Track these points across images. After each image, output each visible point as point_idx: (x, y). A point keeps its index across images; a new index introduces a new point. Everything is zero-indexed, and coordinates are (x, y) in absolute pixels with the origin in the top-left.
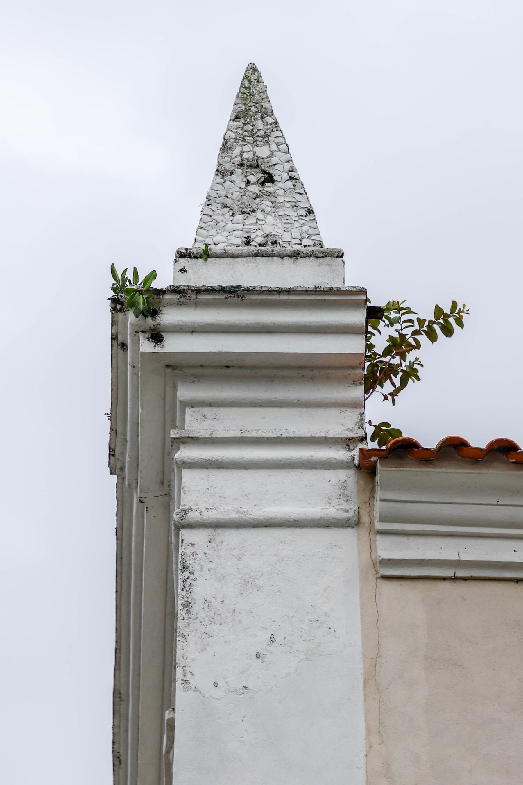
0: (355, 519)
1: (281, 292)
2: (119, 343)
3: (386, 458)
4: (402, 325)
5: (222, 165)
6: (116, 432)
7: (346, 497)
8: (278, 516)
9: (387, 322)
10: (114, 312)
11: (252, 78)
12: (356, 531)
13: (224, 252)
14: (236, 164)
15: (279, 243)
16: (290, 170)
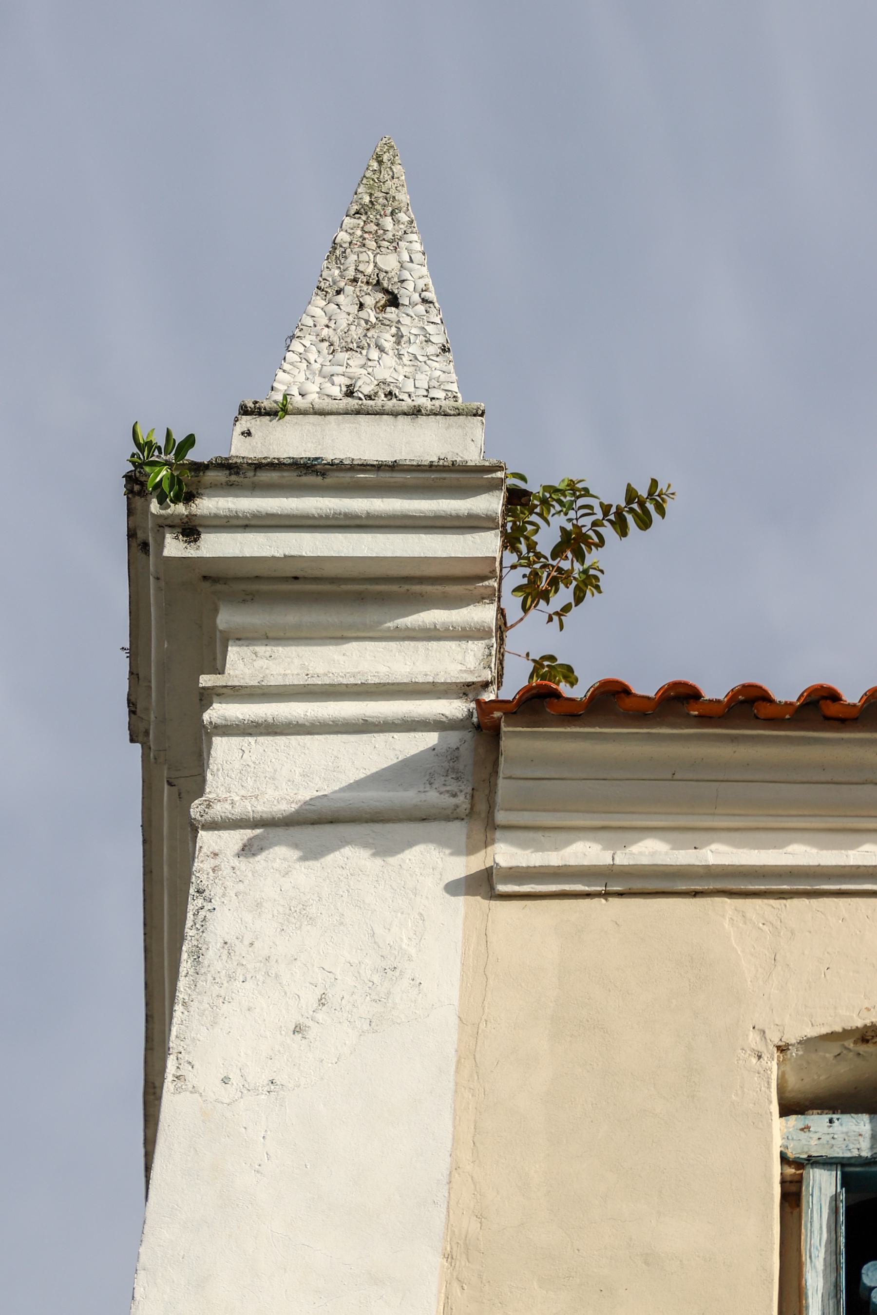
0: (465, 806)
1: (380, 467)
2: (138, 542)
3: (515, 713)
4: (578, 513)
5: (326, 280)
6: (138, 677)
7: (457, 773)
8: (350, 806)
9: (558, 508)
10: (130, 496)
11: (385, 158)
12: (466, 825)
13: (311, 406)
14: (346, 279)
15: (395, 394)
16: (424, 289)
